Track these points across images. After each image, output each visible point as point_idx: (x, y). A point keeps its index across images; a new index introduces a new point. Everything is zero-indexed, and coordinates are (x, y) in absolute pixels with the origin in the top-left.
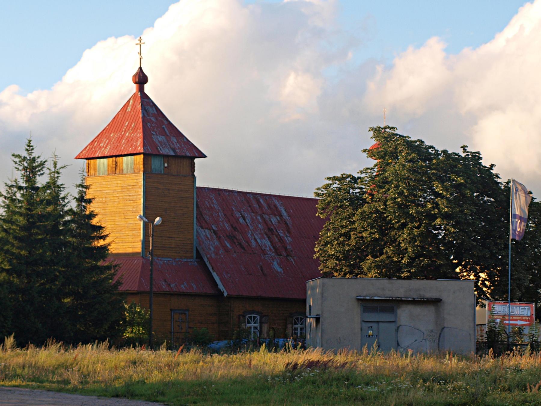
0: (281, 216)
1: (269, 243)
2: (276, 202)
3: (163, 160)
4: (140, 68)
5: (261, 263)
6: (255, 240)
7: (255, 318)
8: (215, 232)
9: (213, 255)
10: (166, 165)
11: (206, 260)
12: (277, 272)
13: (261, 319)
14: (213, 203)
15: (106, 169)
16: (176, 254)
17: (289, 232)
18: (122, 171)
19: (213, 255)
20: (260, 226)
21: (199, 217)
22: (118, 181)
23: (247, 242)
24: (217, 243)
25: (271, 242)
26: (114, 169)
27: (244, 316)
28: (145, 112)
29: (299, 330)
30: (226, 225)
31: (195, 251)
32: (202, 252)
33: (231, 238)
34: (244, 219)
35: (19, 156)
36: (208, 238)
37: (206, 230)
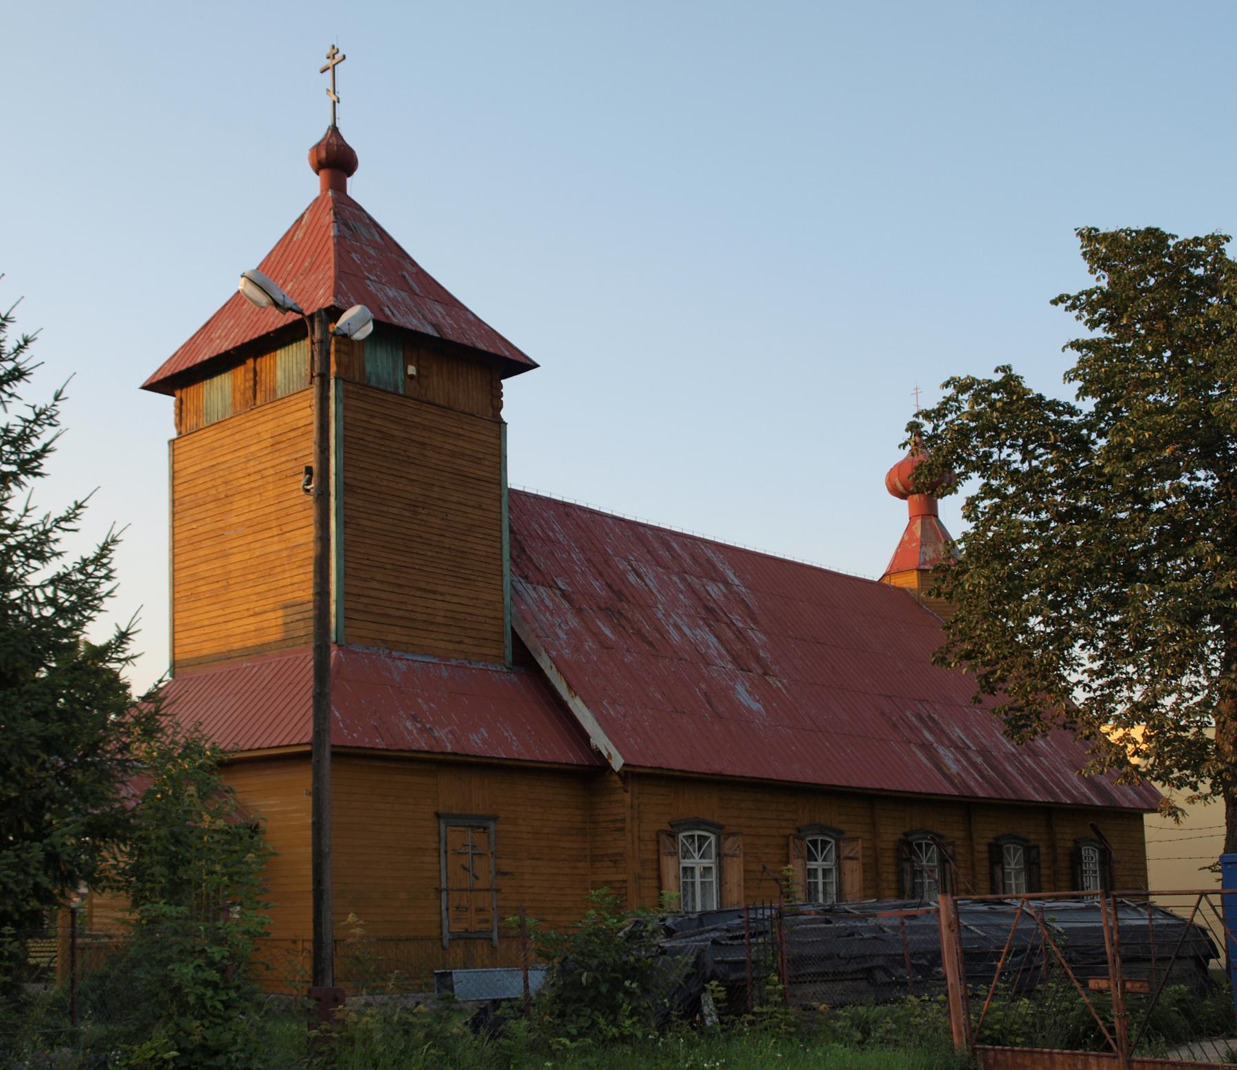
0: (726, 582)
1: (715, 640)
2: (709, 554)
3: (401, 353)
4: (334, 130)
5: (703, 686)
6: (676, 626)
7: (702, 839)
8: (564, 595)
9: (566, 652)
10: (412, 370)
11: (545, 663)
12: (750, 711)
13: (719, 845)
14: (553, 531)
15: (229, 401)
16: (451, 646)
17: (755, 621)
18: (273, 398)
19: (566, 652)
20: (681, 597)
21: (515, 553)
22: (265, 425)
23: (658, 630)
24: (574, 622)
25: (717, 637)
26: (250, 393)
27: (673, 836)
28: (344, 228)
29: (820, 873)
30: (596, 584)
31: (508, 641)
32: (530, 643)
33: (610, 612)
34: (639, 575)
35: (36, 474)
36: (546, 606)
37: (541, 589)
